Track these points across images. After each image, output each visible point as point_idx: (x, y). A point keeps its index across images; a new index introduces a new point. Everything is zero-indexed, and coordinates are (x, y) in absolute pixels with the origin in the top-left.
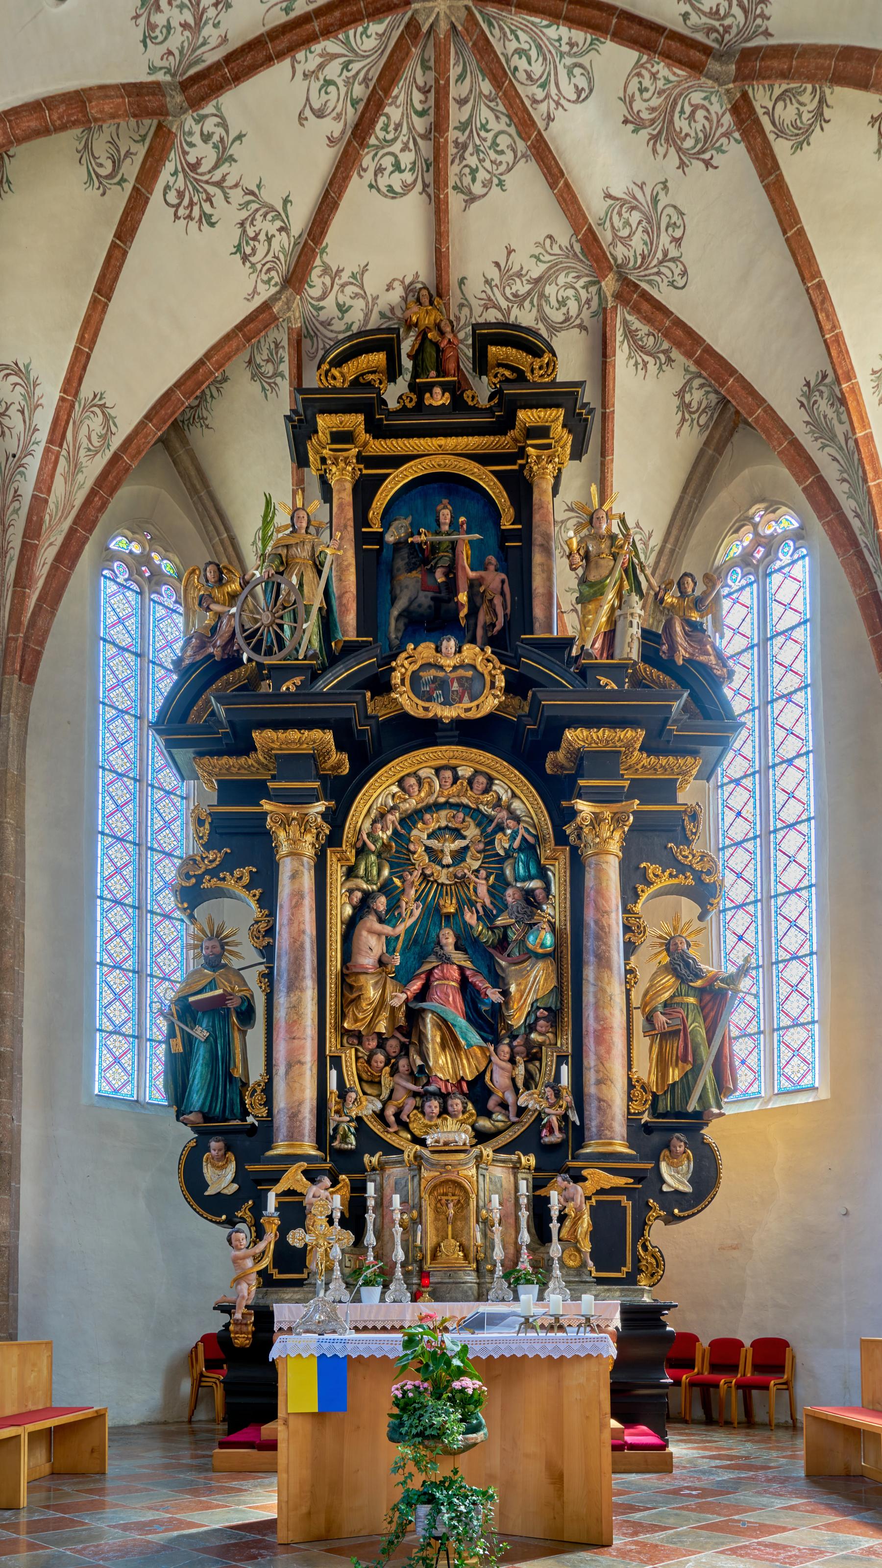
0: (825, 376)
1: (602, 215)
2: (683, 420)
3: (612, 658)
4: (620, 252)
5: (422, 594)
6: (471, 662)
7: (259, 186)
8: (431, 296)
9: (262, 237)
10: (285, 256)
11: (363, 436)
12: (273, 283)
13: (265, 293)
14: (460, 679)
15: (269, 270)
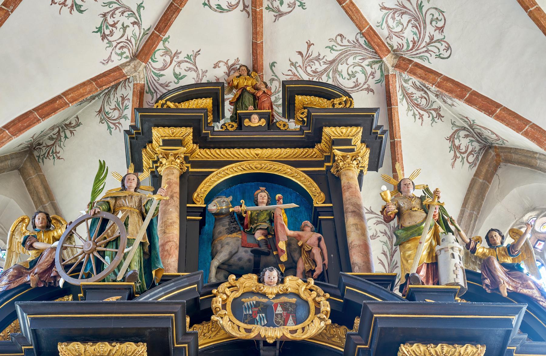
1: (380, 20)
2: (456, 157)
3: (438, 284)
4: (395, 42)
5: (241, 249)
6: (294, 291)
8: (248, 71)
9: (119, 25)
11: (191, 146)
12: (124, 56)
13: (117, 61)
14: (283, 305)
15: (122, 47)
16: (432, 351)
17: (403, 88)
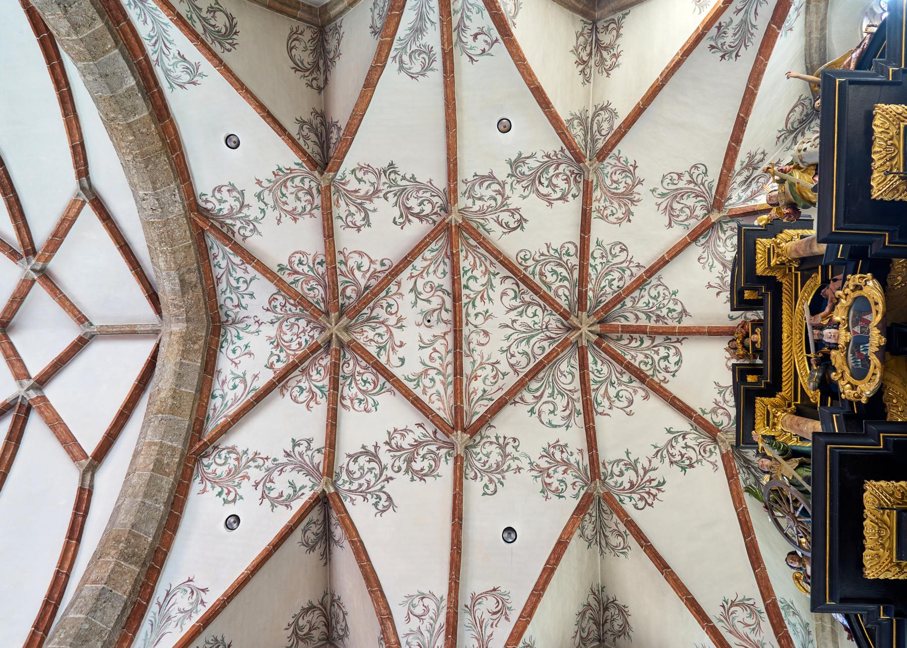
0: (712, 47)
1: (682, 227)
4: (700, 212)
7: (655, 447)
9: (683, 451)
10: (701, 438)
12: (713, 450)
13: (717, 457)
15: (705, 451)
16: (878, 163)
17: (746, 200)
